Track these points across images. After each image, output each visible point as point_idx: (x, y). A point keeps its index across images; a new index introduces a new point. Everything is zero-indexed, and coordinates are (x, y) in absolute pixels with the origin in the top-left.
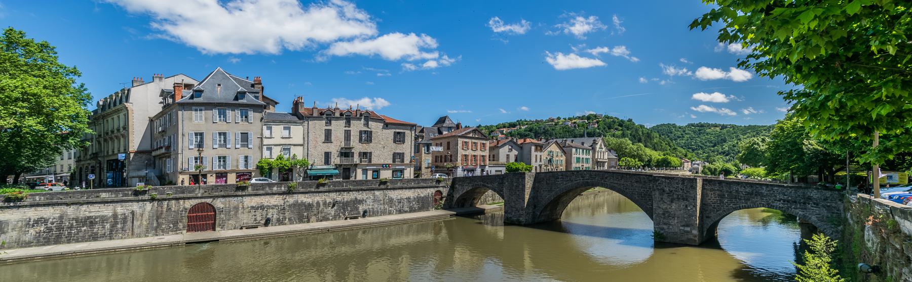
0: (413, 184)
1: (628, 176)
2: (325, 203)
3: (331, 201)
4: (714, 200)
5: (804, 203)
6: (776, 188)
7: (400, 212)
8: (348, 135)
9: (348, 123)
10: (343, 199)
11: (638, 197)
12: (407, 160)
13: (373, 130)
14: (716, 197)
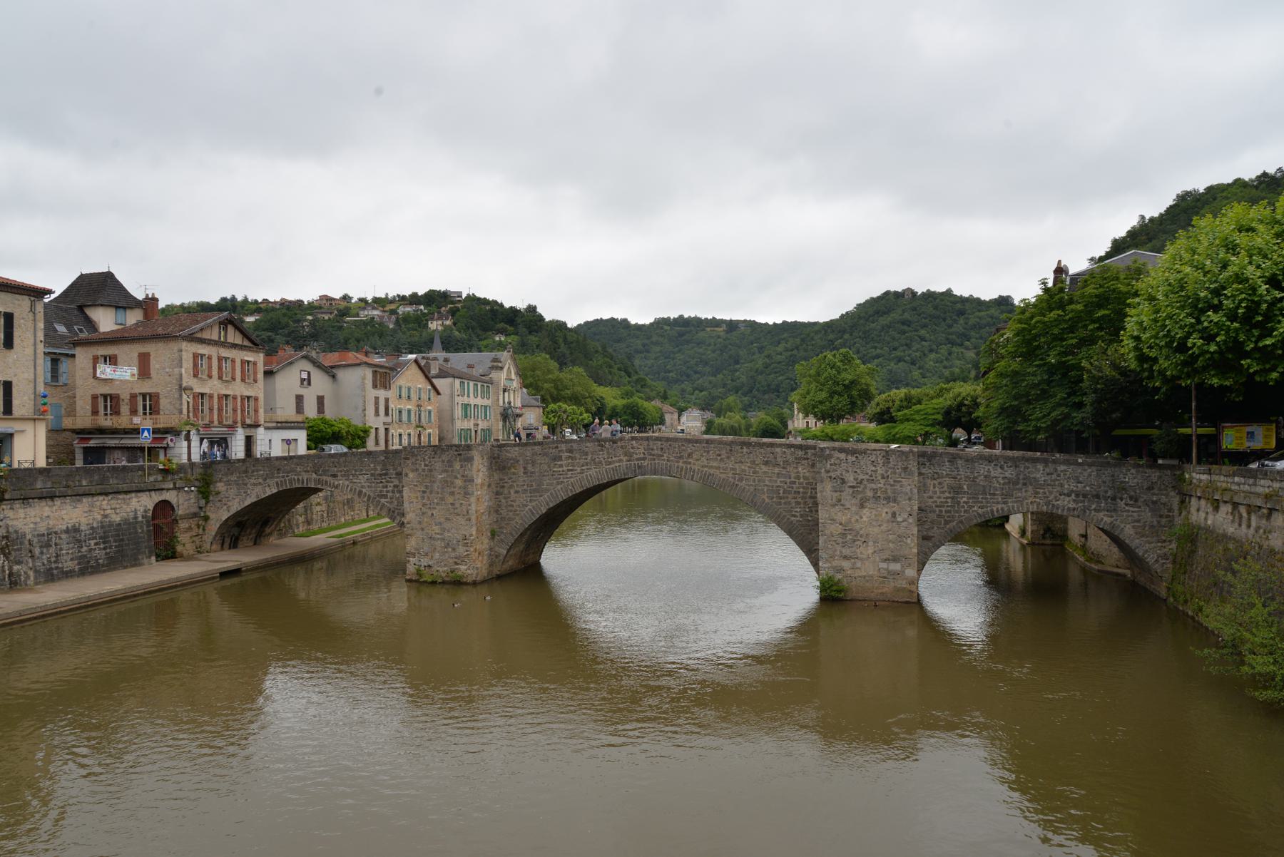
0: (84, 483)
1: (745, 450)
4: (939, 497)
5: (1114, 499)
6: (1063, 467)
7: (51, 576)
11: (768, 497)
14: (943, 493)
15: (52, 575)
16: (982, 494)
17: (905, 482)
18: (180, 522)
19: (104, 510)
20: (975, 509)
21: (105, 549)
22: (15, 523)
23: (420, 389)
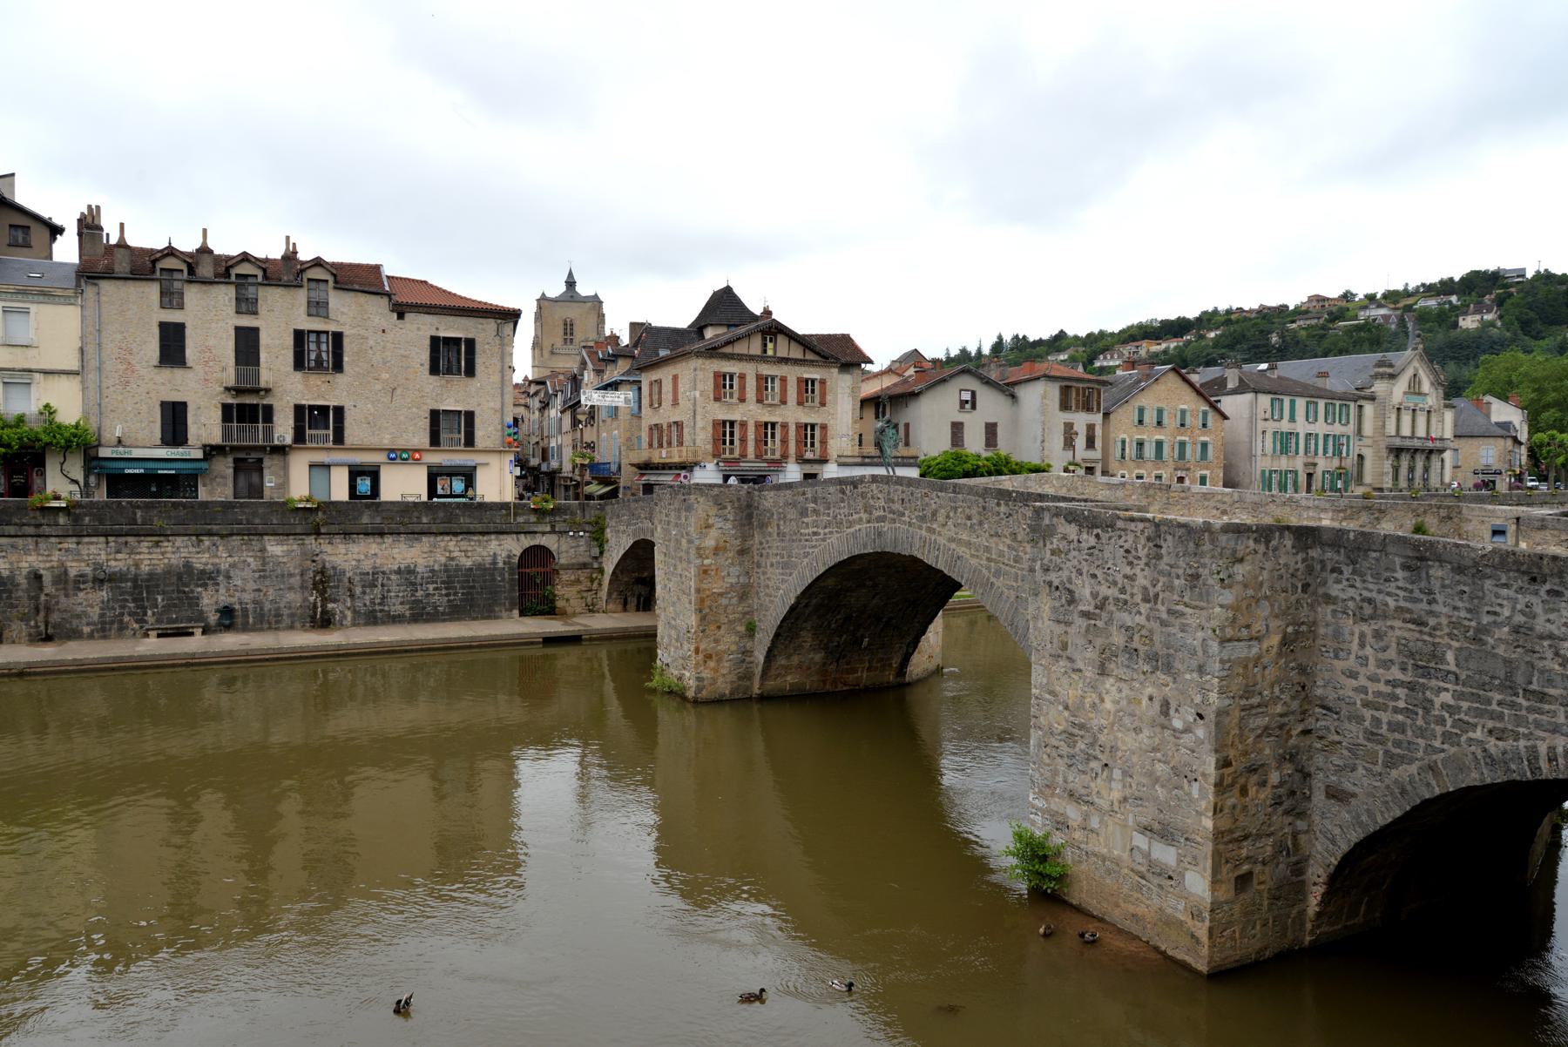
2: (61, 578)
3: (88, 570)
4: (1373, 679)
7: (372, 618)
8: (247, 345)
9: (246, 305)
10: (137, 565)
12: (486, 432)
13: (347, 331)
15: (375, 618)
16: (1502, 688)
17: (1192, 617)
18: (561, 572)
19: (450, 552)
20: (1478, 734)
21: (447, 595)
22: (332, 558)
23: (1183, 412)
